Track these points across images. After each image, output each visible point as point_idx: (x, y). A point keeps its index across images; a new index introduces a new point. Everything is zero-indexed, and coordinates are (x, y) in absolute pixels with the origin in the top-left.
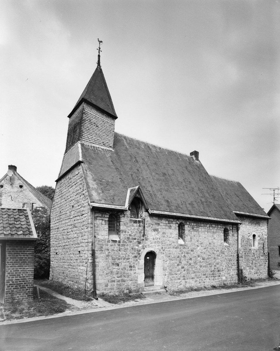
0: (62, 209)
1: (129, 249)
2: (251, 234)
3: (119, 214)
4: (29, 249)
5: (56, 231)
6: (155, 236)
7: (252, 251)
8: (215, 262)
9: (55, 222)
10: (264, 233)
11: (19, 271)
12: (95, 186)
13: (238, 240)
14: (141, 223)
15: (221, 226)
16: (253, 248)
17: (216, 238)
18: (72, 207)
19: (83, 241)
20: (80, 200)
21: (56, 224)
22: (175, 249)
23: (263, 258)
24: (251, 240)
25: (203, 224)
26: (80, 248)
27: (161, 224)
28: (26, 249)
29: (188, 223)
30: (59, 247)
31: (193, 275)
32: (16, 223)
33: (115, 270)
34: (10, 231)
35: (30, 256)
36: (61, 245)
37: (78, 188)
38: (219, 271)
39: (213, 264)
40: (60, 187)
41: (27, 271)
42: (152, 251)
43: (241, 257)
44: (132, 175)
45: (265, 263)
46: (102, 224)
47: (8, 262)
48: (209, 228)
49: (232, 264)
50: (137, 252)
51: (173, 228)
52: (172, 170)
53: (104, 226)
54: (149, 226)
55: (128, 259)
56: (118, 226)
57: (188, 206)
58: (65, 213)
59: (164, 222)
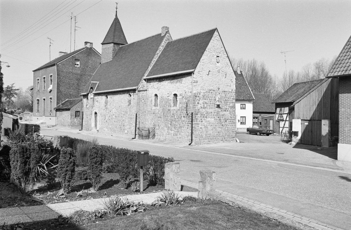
23: (185, 119)
38: (124, 126)
43: (160, 117)
45: (188, 125)
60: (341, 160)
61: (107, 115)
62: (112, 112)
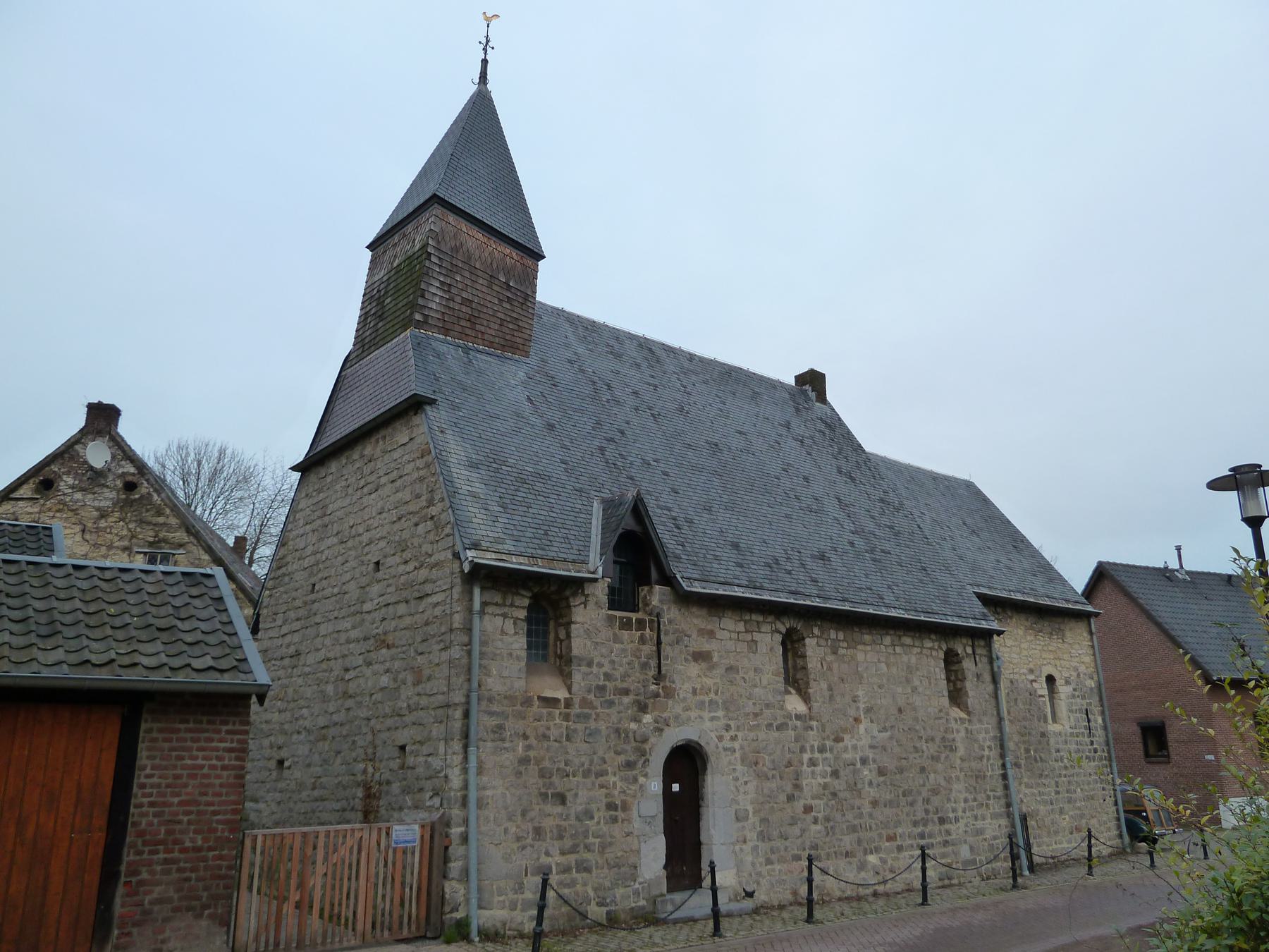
0: (320, 576)
1: (604, 732)
2: (1037, 673)
3: (568, 593)
4: (228, 732)
5: (284, 668)
6: (699, 679)
7: (1052, 741)
8: (924, 785)
9: (285, 630)
10: (1082, 669)
11: (180, 822)
12: (479, 488)
13: (996, 696)
14: (648, 629)
15: (933, 641)
16: (1055, 728)
17: (920, 690)
18: (371, 567)
19: (424, 701)
20: (416, 541)
21: (288, 639)
22: (776, 734)
24: (1043, 696)
25: (870, 633)
26: (406, 732)
27: (720, 634)
28: (219, 732)
29: (816, 631)
30: (295, 737)
31: (848, 841)
32: (179, 623)
33: (548, 823)
34: (163, 655)
35: (230, 760)
36: (307, 723)
37: (406, 495)
39: (920, 793)
40: (319, 491)
41: (214, 825)
42: (690, 741)
44: (602, 449)
46: (502, 630)
47: (143, 786)
48: (890, 650)
49: (988, 793)
50: (634, 744)
51: (762, 648)
52: (740, 433)
53: (510, 640)
54: (678, 643)
55: (602, 773)
56: (561, 641)
57: (810, 563)
58: (336, 590)
59: (729, 625)
61: (813, 763)
62: (848, 741)
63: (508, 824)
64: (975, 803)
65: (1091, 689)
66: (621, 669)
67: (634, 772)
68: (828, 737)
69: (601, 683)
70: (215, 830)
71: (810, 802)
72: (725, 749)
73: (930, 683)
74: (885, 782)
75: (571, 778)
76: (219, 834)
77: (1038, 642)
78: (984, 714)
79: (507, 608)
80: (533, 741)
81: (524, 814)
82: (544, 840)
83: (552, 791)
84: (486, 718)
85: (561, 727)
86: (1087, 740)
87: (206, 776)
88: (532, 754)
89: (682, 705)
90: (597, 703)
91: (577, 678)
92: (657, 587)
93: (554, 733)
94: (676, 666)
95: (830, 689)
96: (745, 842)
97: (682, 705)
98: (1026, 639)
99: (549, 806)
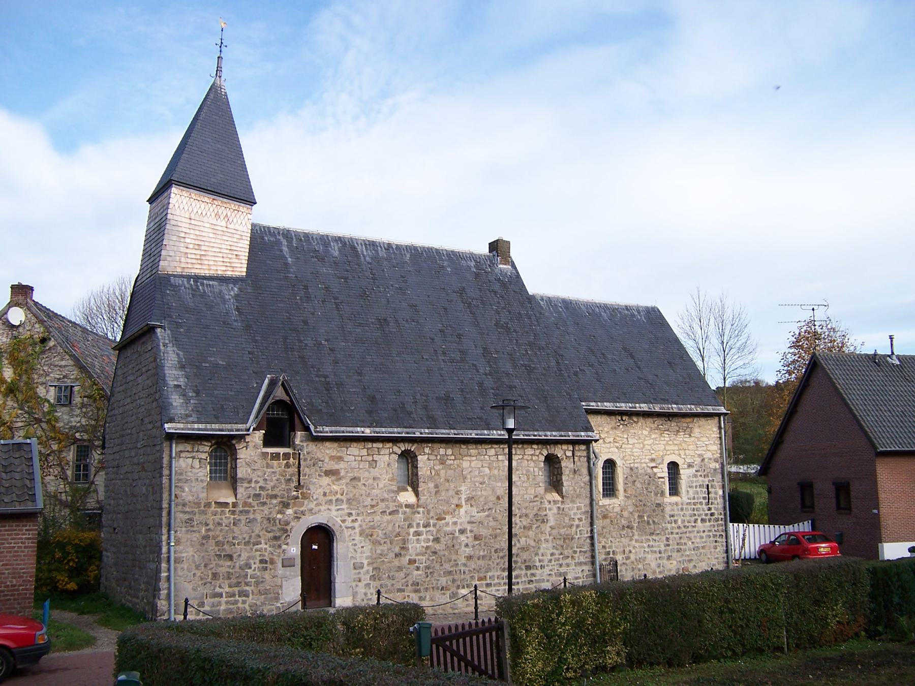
4: (27, 530)
6: (329, 487)
12: (182, 381)
14: (291, 459)
27: (347, 458)
33: (222, 570)
43: (628, 527)
46: (192, 466)
50: (279, 526)
54: (314, 465)
60: (725, 555)
61: (418, 534)
63: (196, 571)
64: (562, 556)
65: (715, 470)
66: (272, 483)
67: (279, 542)
68: (432, 517)
69: (257, 492)
70: (22, 577)
71: (413, 557)
72: (347, 528)
73: (528, 479)
74: (480, 544)
75: (236, 546)
76: (24, 579)
77: (663, 439)
78: (578, 496)
79: (195, 453)
80: (211, 526)
81: (206, 566)
82: (219, 580)
83: (225, 553)
84: (181, 515)
85: (229, 519)
86: (706, 507)
87: (17, 552)
88: (210, 533)
89: (315, 503)
90: (254, 503)
91: (240, 490)
92: (299, 433)
93: (225, 522)
94: (311, 480)
95: (436, 486)
96: (360, 581)
97: (315, 503)
98: (650, 437)
99: (222, 561)
